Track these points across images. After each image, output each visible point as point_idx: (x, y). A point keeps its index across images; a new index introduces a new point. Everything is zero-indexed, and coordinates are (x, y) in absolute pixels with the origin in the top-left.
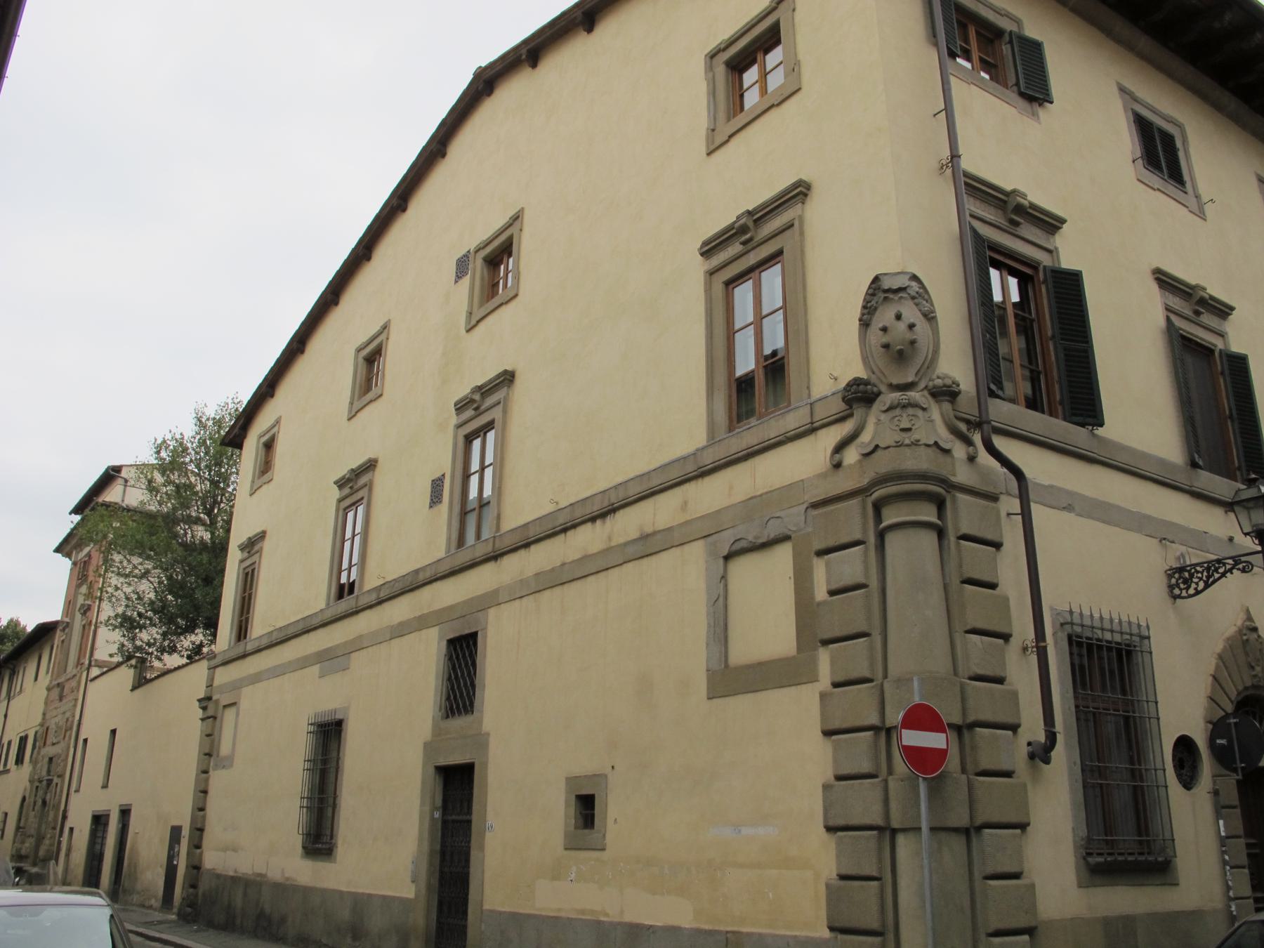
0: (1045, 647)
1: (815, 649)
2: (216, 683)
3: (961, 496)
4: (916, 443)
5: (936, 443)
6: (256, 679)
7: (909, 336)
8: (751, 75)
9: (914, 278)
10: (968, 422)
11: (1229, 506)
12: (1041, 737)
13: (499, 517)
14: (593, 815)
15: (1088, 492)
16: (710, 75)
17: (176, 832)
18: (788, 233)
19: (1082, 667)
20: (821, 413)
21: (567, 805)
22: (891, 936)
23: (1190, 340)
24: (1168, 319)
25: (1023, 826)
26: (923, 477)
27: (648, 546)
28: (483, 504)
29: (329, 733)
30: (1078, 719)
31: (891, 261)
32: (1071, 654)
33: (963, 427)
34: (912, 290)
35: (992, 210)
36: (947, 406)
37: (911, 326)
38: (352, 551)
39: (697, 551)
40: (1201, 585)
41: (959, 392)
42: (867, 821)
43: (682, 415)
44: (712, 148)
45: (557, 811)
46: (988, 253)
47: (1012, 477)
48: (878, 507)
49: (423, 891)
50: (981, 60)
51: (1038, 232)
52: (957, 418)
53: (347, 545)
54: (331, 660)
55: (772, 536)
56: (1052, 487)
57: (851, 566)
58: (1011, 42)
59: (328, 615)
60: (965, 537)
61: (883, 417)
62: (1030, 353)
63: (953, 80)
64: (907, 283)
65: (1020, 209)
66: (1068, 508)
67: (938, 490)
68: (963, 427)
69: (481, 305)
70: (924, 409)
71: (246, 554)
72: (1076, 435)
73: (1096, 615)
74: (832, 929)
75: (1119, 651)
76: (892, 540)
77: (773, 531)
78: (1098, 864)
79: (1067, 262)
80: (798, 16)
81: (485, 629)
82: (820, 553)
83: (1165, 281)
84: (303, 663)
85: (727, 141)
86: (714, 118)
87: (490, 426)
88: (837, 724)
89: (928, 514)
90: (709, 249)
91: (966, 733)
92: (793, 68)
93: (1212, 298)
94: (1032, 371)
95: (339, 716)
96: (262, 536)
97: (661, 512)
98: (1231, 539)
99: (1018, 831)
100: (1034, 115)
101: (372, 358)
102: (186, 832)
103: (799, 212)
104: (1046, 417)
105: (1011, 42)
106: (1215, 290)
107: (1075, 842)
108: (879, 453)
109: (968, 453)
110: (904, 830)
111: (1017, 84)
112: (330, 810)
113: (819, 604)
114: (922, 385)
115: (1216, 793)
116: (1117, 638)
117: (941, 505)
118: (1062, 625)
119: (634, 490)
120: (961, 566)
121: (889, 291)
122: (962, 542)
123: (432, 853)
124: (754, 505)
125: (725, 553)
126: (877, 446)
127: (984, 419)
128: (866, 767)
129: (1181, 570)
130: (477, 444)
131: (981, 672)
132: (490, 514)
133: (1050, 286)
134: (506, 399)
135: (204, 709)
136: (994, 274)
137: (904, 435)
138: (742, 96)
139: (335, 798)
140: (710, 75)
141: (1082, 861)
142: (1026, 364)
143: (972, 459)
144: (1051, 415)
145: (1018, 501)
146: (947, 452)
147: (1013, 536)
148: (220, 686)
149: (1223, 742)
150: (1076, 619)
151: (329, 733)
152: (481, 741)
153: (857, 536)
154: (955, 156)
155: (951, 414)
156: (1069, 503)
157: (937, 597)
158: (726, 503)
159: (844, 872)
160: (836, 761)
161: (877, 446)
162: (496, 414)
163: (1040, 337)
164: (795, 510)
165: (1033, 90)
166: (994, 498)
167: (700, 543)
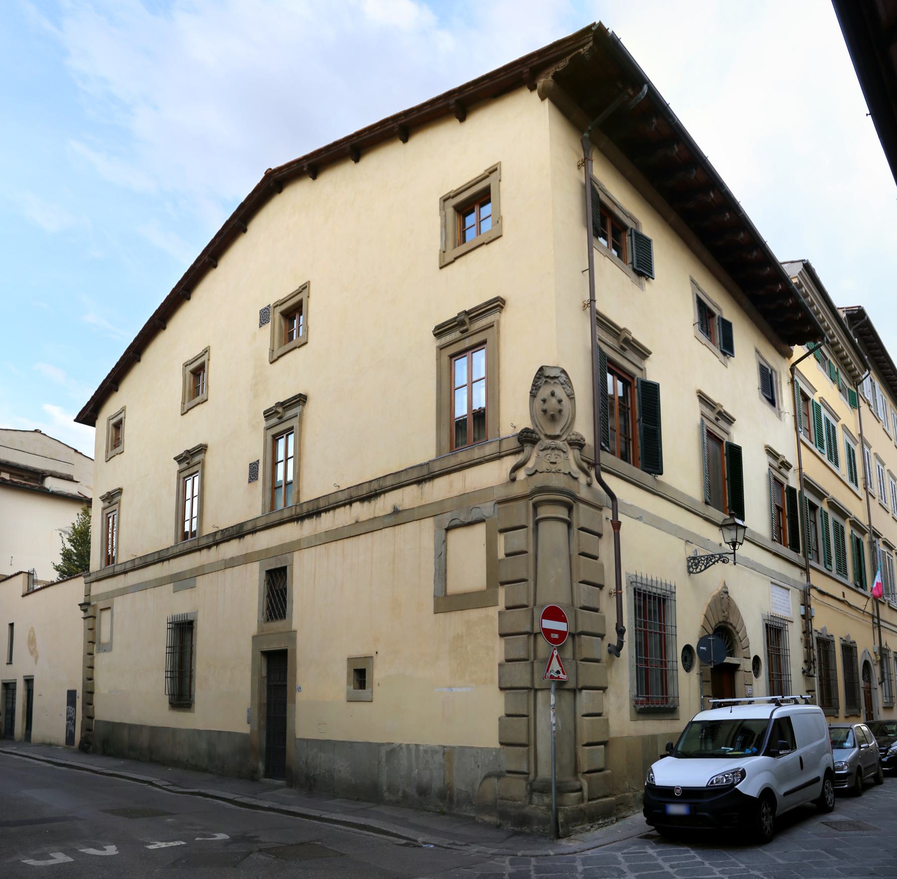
2: (93, 593)
3: (581, 505)
4: (558, 472)
6: (124, 591)
7: (558, 407)
8: (471, 220)
9: (563, 371)
10: (588, 463)
11: (721, 526)
12: (615, 643)
13: (299, 492)
14: (365, 681)
15: (651, 511)
16: (443, 213)
17: (71, 695)
18: (489, 330)
20: (506, 447)
21: (348, 676)
22: (532, 747)
23: (711, 434)
24: (702, 420)
25: (604, 689)
27: (397, 517)
28: (288, 484)
29: (183, 631)
34: (561, 378)
35: (611, 338)
36: (577, 452)
38: (191, 509)
39: (429, 523)
40: (703, 567)
41: (585, 445)
42: (522, 684)
43: (423, 446)
44: (443, 264)
45: (340, 680)
46: (608, 364)
48: (536, 506)
49: (256, 729)
50: (613, 242)
51: (636, 357)
52: (583, 460)
53: (188, 503)
54: (182, 581)
56: (632, 505)
57: (519, 540)
58: (631, 235)
59: (176, 550)
61: (541, 453)
62: (626, 427)
63: (595, 251)
64: (559, 374)
65: (626, 341)
67: (570, 501)
68: (585, 465)
69: (280, 347)
71: (107, 504)
72: (646, 478)
73: (649, 579)
74: (501, 744)
75: (659, 599)
76: (543, 526)
77: (475, 515)
79: (651, 377)
80: (503, 185)
81: (292, 565)
83: (703, 399)
84: (159, 582)
85: (453, 262)
86: (445, 242)
87: (290, 431)
89: (562, 513)
90: (440, 331)
91: (577, 639)
92: (498, 221)
93: (725, 412)
95: (190, 618)
96: (120, 491)
97: (407, 498)
98: (721, 545)
100: (641, 286)
101: (197, 373)
102: (80, 694)
103: (497, 318)
104: (631, 466)
105: (631, 235)
106: (728, 408)
110: (541, 690)
111: (632, 263)
112: (188, 679)
113: (500, 561)
114: (564, 437)
115: (701, 674)
116: (659, 592)
117: (570, 509)
119: (389, 482)
120: (579, 545)
123: (260, 705)
124: (464, 500)
126: (536, 471)
128: (522, 655)
129: (694, 558)
130: (281, 442)
131: (586, 605)
132: (293, 490)
134: (301, 414)
135: (85, 611)
136: (610, 377)
137: (552, 466)
138: (464, 232)
139: (191, 671)
140: (443, 213)
143: (589, 485)
146: (576, 479)
147: (607, 528)
148: (97, 596)
149: (704, 648)
150: (639, 580)
151: (183, 631)
152: (291, 636)
153: (523, 523)
154: (592, 300)
155: (579, 457)
156: (640, 516)
157: (564, 561)
158: (448, 496)
160: (506, 651)
161: (536, 471)
162: (294, 423)
163: (632, 422)
164: (488, 504)
165: (643, 269)
166: (600, 509)
167: (431, 519)
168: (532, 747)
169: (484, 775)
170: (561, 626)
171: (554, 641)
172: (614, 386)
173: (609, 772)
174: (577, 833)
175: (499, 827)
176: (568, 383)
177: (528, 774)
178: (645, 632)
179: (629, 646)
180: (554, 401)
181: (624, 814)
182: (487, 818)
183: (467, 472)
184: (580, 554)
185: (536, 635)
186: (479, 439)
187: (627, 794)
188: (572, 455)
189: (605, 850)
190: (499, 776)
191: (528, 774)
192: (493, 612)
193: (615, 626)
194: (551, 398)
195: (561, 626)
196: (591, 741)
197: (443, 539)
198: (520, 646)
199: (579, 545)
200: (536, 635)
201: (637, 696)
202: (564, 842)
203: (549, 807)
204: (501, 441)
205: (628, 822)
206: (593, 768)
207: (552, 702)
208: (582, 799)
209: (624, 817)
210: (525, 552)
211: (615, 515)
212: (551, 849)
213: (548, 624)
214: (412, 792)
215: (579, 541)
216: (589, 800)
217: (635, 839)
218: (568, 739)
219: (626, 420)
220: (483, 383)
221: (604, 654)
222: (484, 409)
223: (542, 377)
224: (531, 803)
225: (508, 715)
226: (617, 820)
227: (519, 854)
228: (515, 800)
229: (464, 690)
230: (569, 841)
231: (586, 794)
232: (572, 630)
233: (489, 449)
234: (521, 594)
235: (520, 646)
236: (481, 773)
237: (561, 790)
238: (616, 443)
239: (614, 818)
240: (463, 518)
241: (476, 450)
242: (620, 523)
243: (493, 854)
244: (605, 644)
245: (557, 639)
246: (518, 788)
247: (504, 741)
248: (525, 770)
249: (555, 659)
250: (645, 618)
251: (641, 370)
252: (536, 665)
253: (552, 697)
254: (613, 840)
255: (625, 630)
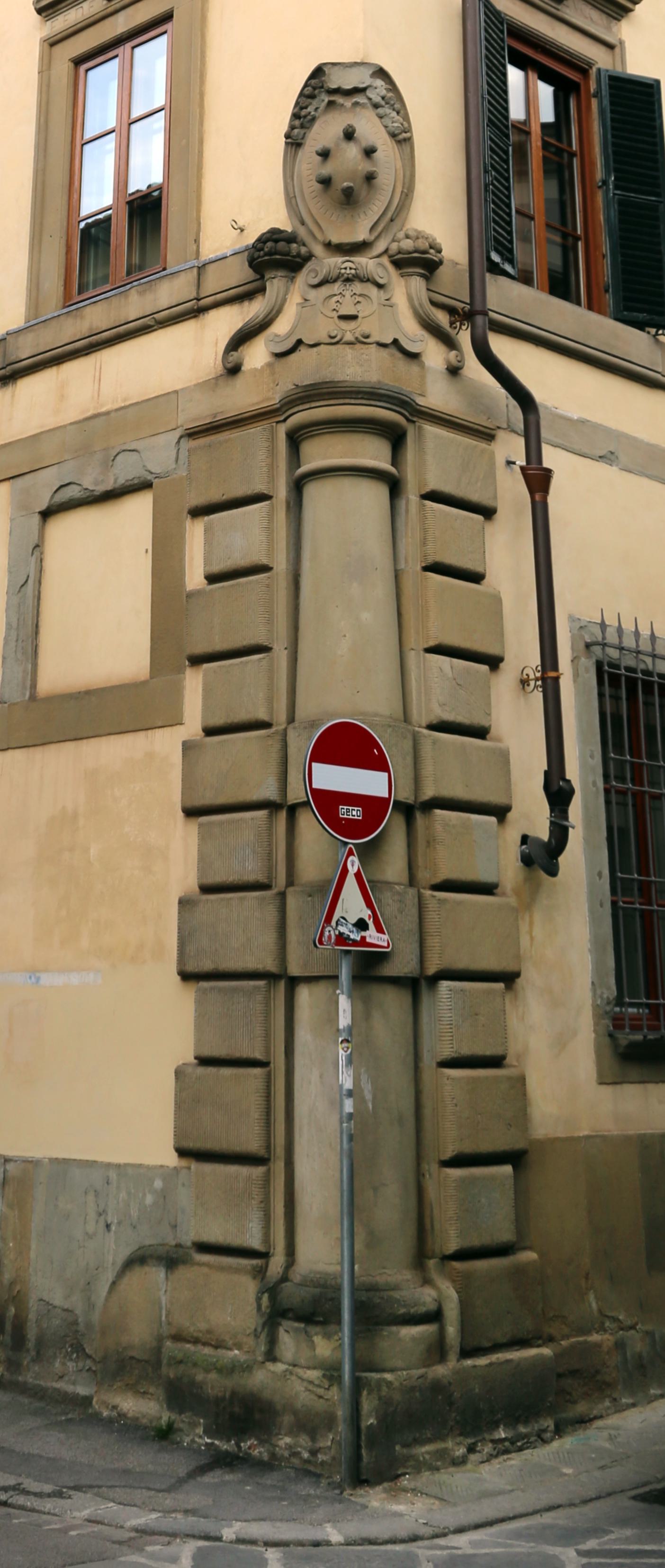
0: (557, 679)
1: (181, 670)
3: (431, 430)
4: (363, 340)
5: (396, 342)
7: (365, 166)
9: (381, 73)
10: (451, 311)
12: (543, 832)
19: (617, 718)
20: (214, 283)
22: (279, 1167)
25: (509, 978)
26: (371, 394)
30: (608, 803)
31: (342, 41)
32: (601, 695)
33: (442, 318)
34: (379, 89)
36: (417, 284)
37: (369, 152)
41: (441, 262)
42: (250, 963)
46: (508, 41)
47: (513, 403)
48: (295, 439)
52: (434, 303)
55: (121, 481)
56: (583, 422)
60: (434, 496)
61: (313, 294)
66: (608, 458)
67: (395, 420)
68: (442, 318)
70: (380, 286)
73: (645, 632)
74: (182, 1153)
76: (313, 492)
77: (125, 471)
78: (632, 1045)
82: (197, 512)
88: (208, 798)
89: (373, 453)
91: (420, 819)
94: (565, 236)
99: (501, 985)
107: (595, 1007)
108: (303, 351)
109: (448, 362)
113: (190, 595)
114: (380, 247)
117: (396, 439)
118: (588, 646)
120: (424, 542)
121: (338, 91)
122: (428, 503)
124: (99, 430)
125: (43, 506)
126: (299, 342)
127: (478, 307)
128: (252, 871)
131: (449, 716)
133: (606, 102)
136: (515, 76)
137: (344, 325)
141: (607, 1040)
142: (557, 224)
143: (454, 371)
144: (590, 308)
145: (522, 441)
146: (414, 357)
147: (512, 492)
150: (612, 637)
153: (259, 486)
155: (424, 296)
157: (380, 588)
159: (207, 1052)
164: (162, 439)
166: (487, 436)
168: (279, 1167)
169: (125, 1253)
170: (371, 783)
171: (349, 829)
172: (529, 98)
173: (529, 1256)
174: (419, 1467)
175: (164, 1435)
176: (393, 100)
177: (264, 1255)
178: (638, 797)
179: (587, 840)
180: (352, 152)
181: (581, 1408)
182: (130, 1404)
183: (109, 357)
184: (426, 569)
185: (292, 810)
186: (141, 268)
187: (595, 1338)
188: (405, 291)
189: (518, 1535)
190: (172, 1260)
191: (264, 1255)
192: (167, 744)
193: (539, 780)
194: (344, 145)
195: (371, 783)
196: (468, 1147)
197: (34, 539)
198: (244, 846)
199: (424, 542)
200: (292, 810)
201: (619, 1001)
202: (375, 1498)
203: (332, 1373)
204: (201, 269)
205: (596, 1436)
206: (475, 1241)
207: (344, 1020)
208: (438, 1350)
209: (583, 1421)
210: (264, 569)
211: (533, 451)
212: (332, 1520)
213: (331, 777)
214: (262, 1205)
215: (425, 530)
216: (466, 1353)
217: (624, 1502)
218: (403, 1144)
219: (565, 187)
220: (159, 121)
221: (508, 868)
222: (160, 188)
223: (321, 90)
224: (271, 1356)
225: (204, 1061)
226: (559, 1431)
227: (228, 1533)
228: (219, 1345)
229: (75, 979)
230: (395, 1494)
231: (452, 1331)
232: (405, 794)
233: (168, 293)
234: (250, 688)
235: (244, 846)
236: (116, 1250)
237: (374, 1314)
238: (537, 250)
239: (549, 1423)
240: (92, 480)
241: (134, 296)
242: (547, 475)
243: (143, 1531)
244: (512, 835)
245: (358, 823)
246: (229, 1304)
247: (190, 1144)
248: (255, 1242)
249: (351, 883)
250: (635, 751)
251: (610, 47)
252: (292, 902)
253: (344, 1003)
254: (546, 1499)
255: (572, 792)
